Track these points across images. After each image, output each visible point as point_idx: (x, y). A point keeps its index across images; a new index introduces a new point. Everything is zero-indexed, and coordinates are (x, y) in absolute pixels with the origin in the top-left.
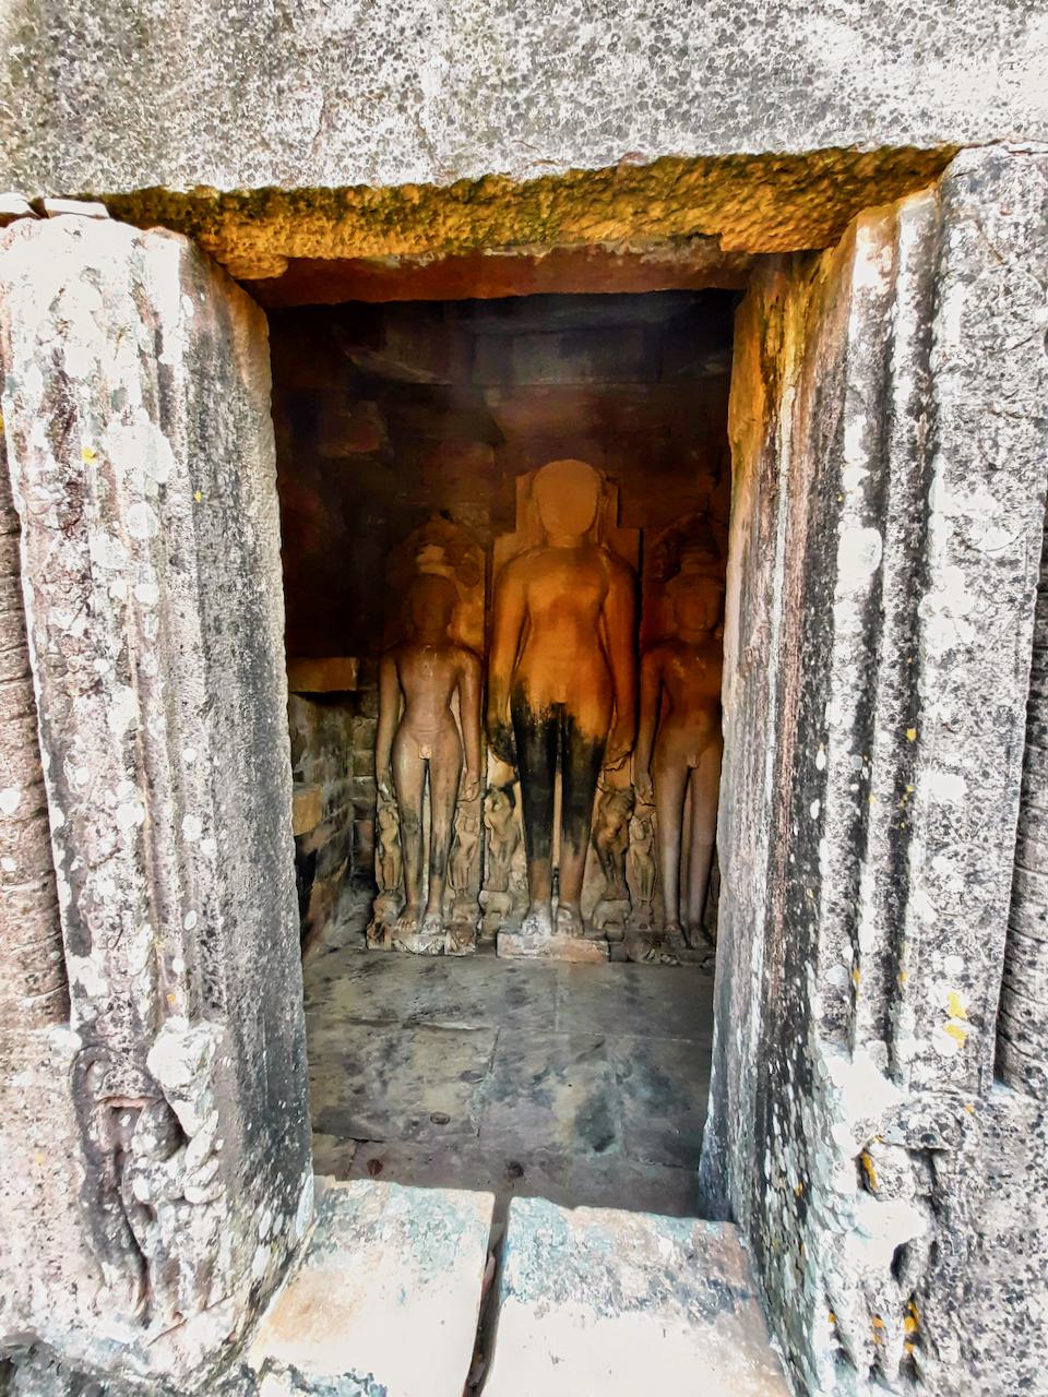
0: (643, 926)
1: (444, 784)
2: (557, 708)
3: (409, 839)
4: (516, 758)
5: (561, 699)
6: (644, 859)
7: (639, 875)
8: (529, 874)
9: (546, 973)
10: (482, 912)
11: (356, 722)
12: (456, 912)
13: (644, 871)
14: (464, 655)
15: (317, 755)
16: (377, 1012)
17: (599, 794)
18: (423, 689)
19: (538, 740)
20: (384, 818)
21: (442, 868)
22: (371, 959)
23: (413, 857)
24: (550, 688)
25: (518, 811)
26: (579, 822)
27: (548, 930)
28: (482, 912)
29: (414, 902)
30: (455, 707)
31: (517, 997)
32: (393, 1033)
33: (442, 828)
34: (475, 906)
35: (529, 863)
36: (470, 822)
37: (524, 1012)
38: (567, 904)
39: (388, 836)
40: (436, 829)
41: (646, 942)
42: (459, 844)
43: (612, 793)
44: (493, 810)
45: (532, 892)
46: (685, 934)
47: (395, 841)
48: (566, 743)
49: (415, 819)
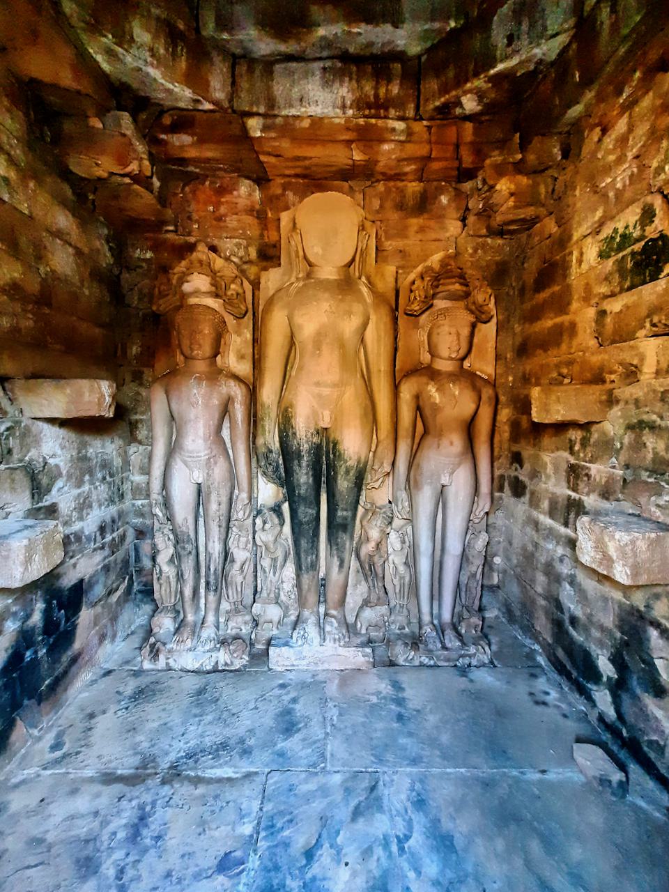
0: (402, 628)
1: (215, 506)
2: (323, 432)
3: (184, 560)
4: (286, 480)
5: (325, 423)
6: (402, 569)
7: (396, 582)
8: (299, 585)
9: (313, 685)
10: (256, 623)
11: (133, 449)
12: (231, 624)
13: (402, 578)
14: (232, 383)
15: (80, 484)
16: (136, 761)
17: (360, 511)
18: (192, 416)
19: (304, 464)
20: (159, 540)
21: (219, 583)
22: (143, 681)
23: (189, 576)
24: (315, 415)
25: (287, 528)
26: (344, 537)
27: (317, 640)
28: (256, 623)
29: (190, 618)
30: (225, 433)
31: (288, 724)
32: (143, 795)
33: (216, 548)
34: (248, 618)
35: (298, 576)
36: (243, 540)
37: (292, 744)
38: (333, 612)
39: (163, 559)
40: (210, 549)
41: (406, 644)
42: (233, 561)
43: (373, 510)
44: (263, 529)
45: (301, 601)
46: (440, 630)
47: (171, 561)
48: (332, 467)
49: (189, 541)
